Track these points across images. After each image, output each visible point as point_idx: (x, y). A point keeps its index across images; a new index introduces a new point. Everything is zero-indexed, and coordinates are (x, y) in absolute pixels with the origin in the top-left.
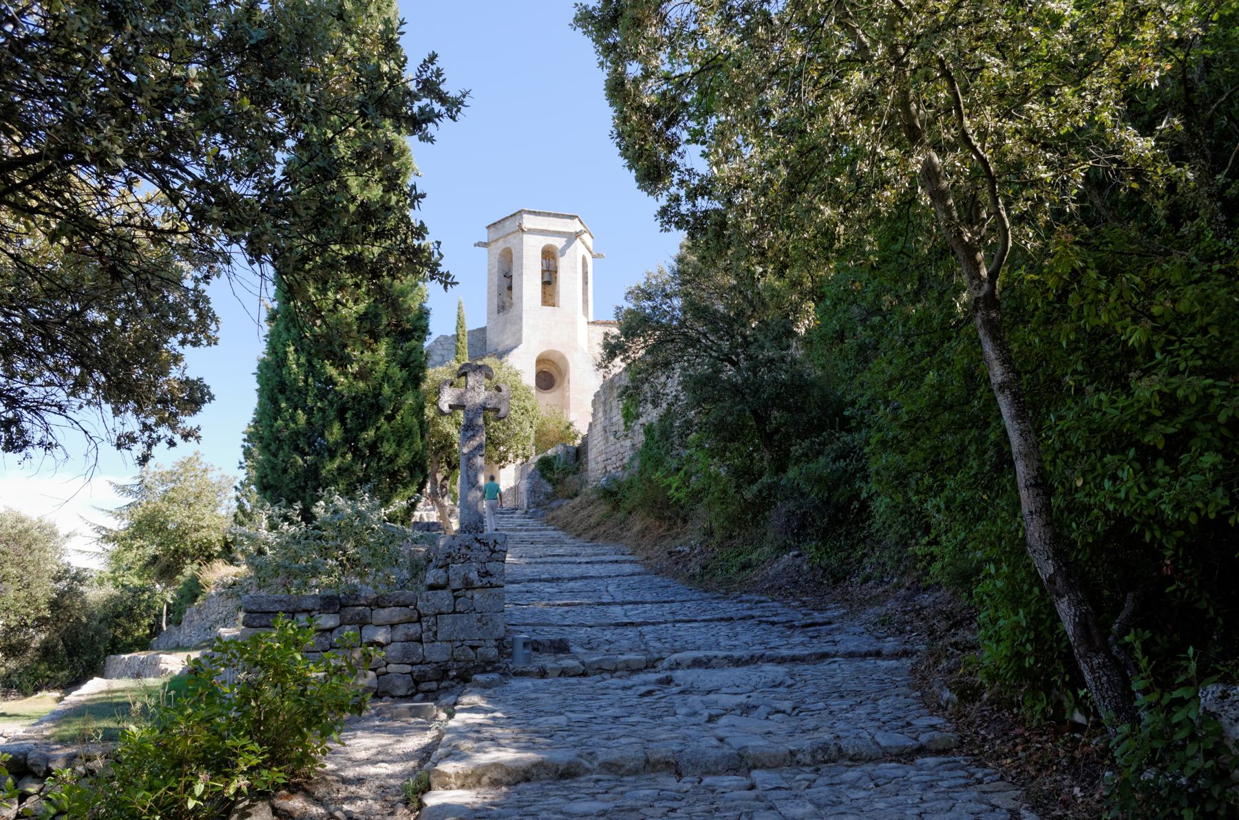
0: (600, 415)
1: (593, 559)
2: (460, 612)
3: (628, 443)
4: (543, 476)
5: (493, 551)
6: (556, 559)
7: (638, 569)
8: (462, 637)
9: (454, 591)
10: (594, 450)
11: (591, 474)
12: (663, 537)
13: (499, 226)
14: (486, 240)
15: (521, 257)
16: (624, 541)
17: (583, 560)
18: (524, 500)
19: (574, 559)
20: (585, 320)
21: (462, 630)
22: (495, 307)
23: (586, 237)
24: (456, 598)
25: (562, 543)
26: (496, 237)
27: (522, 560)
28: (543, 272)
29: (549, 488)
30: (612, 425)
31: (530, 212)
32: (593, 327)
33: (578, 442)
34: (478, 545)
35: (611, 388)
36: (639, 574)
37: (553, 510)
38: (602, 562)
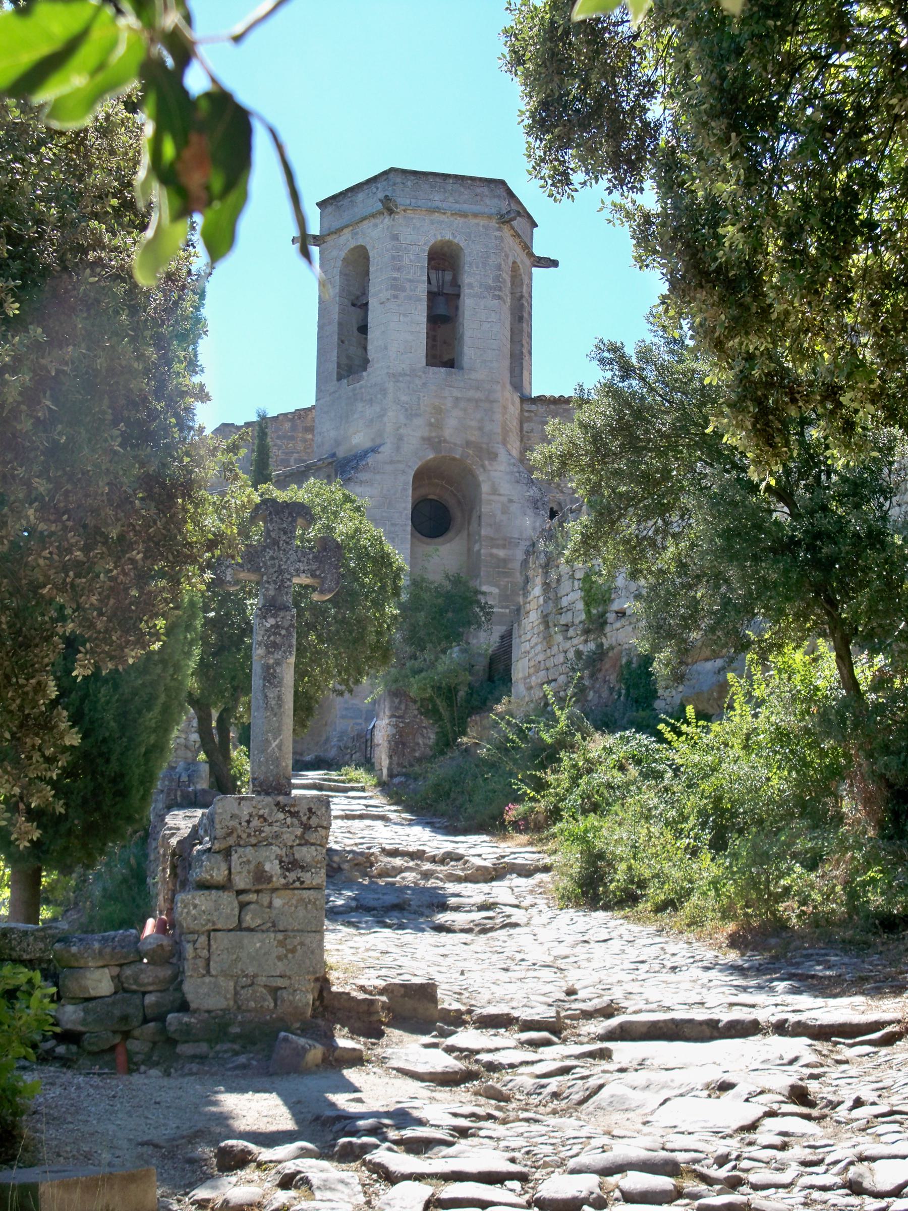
2: (250, 930)
9: (239, 892)
13: (345, 202)
22: (332, 367)
24: (243, 906)
26: (336, 225)
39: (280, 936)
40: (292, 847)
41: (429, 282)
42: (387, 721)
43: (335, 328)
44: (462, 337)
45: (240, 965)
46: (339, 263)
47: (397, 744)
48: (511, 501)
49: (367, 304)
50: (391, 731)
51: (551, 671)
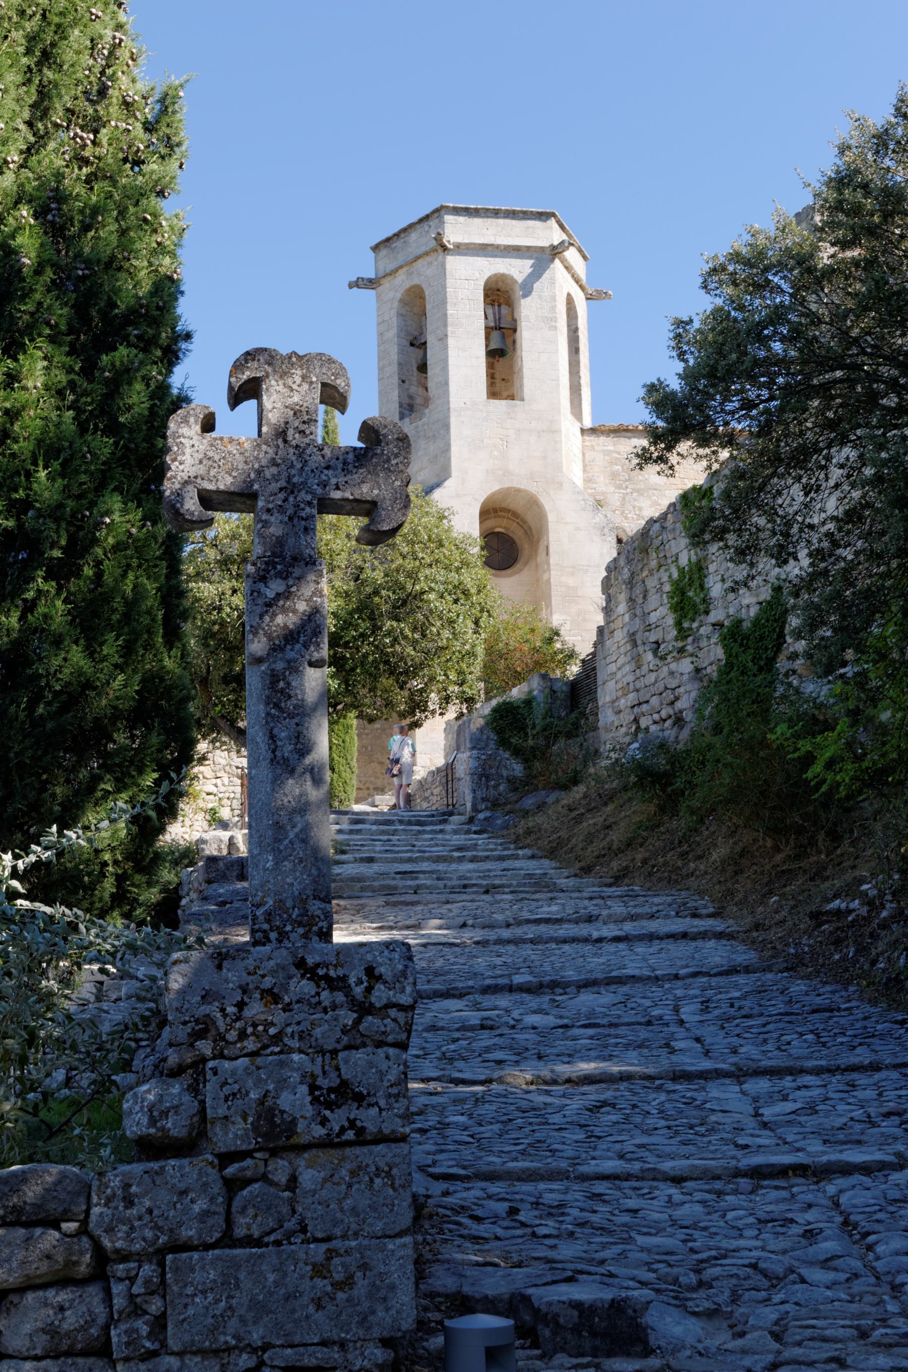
0: (622, 608)
1: (628, 927)
3: (686, 666)
4: (503, 743)
5: (364, 1009)
6: (543, 929)
7: (744, 955)
8: (256, 1336)
9: (226, 1159)
10: (611, 685)
11: (604, 736)
12: (786, 875)
13: (397, 244)
14: (370, 273)
15: (444, 302)
16: (692, 882)
17: (609, 931)
18: (465, 794)
19: (583, 930)
20: (577, 426)
21: (259, 1308)
23: (572, 255)
24: (233, 1186)
25: (553, 888)
26: (391, 267)
27: (468, 936)
28: (488, 330)
29: (517, 768)
30: (648, 628)
31: (457, 211)
32: (591, 440)
33: (574, 669)
34: (306, 987)
35: (645, 551)
36: (748, 970)
37: (526, 813)
38: (651, 937)
39: (318, 1251)
40: (334, 1053)
41: (486, 318)
42: (468, 754)
43: (395, 368)
44: (521, 370)
45: (233, 1324)
46: (396, 304)
47: (480, 777)
48: (578, 529)
49: (425, 343)
50: (473, 764)
51: (642, 692)
